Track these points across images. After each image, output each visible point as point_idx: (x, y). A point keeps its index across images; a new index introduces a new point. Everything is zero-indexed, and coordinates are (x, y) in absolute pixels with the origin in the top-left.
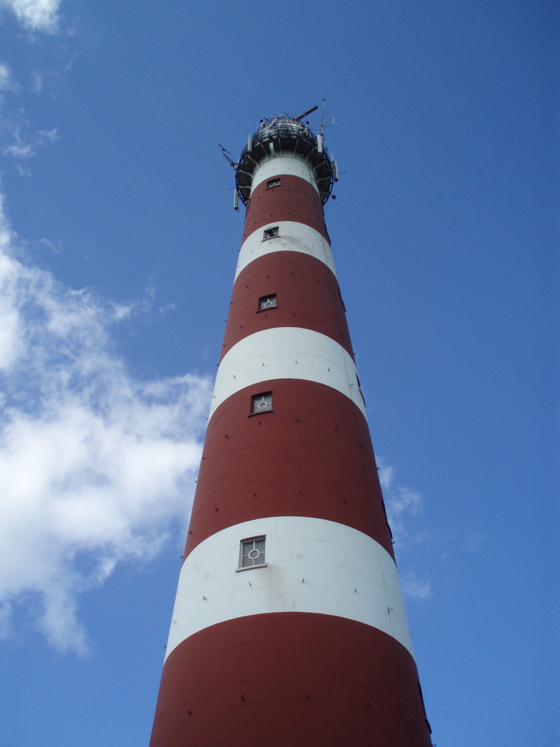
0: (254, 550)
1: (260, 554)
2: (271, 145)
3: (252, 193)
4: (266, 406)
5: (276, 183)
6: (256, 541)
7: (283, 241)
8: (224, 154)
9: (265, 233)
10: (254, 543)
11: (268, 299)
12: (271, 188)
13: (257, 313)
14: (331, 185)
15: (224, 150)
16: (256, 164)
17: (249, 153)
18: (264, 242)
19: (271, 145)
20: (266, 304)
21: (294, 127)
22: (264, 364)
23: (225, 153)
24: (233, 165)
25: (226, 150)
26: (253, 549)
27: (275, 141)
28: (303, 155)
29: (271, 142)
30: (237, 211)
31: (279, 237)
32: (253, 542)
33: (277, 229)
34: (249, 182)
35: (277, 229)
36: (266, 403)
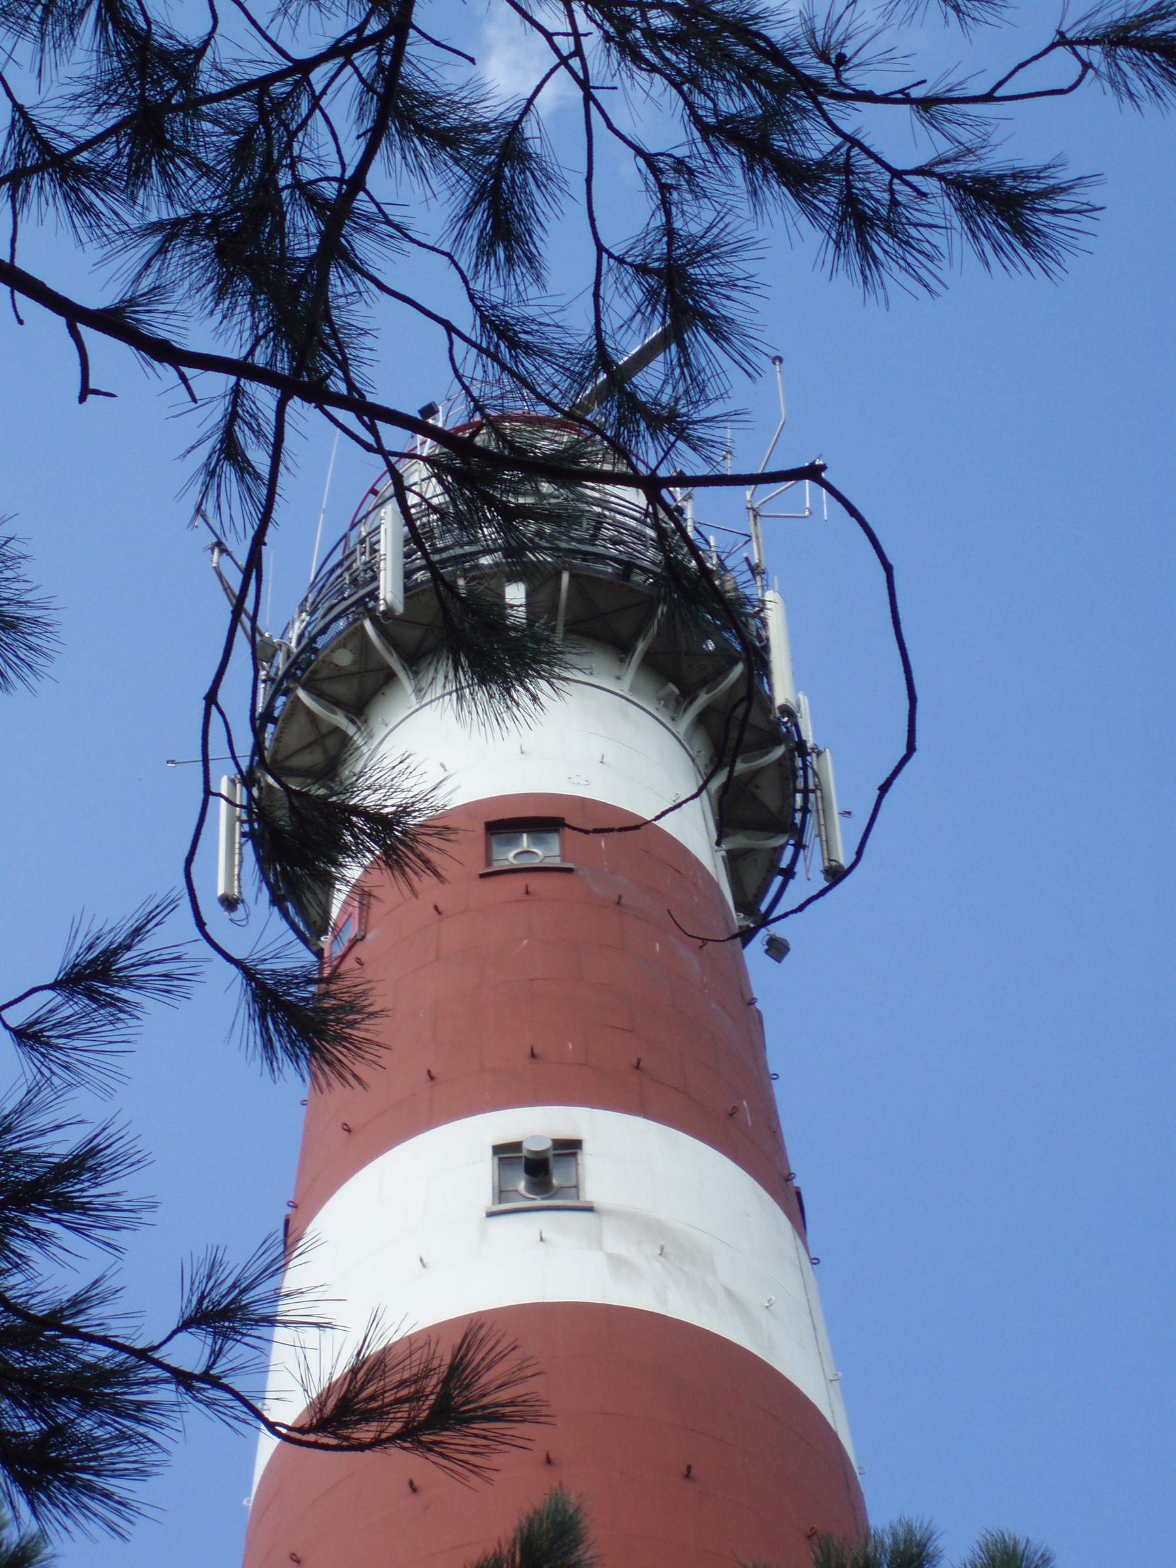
5: (536, 842)
8: (220, 576)
14: (778, 880)
17: (385, 622)
21: (637, 515)
25: (229, 554)
28: (672, 688)
29: (513, 578)
30: (235, 915)
33: (569, 1148)
35: (569, 1148)
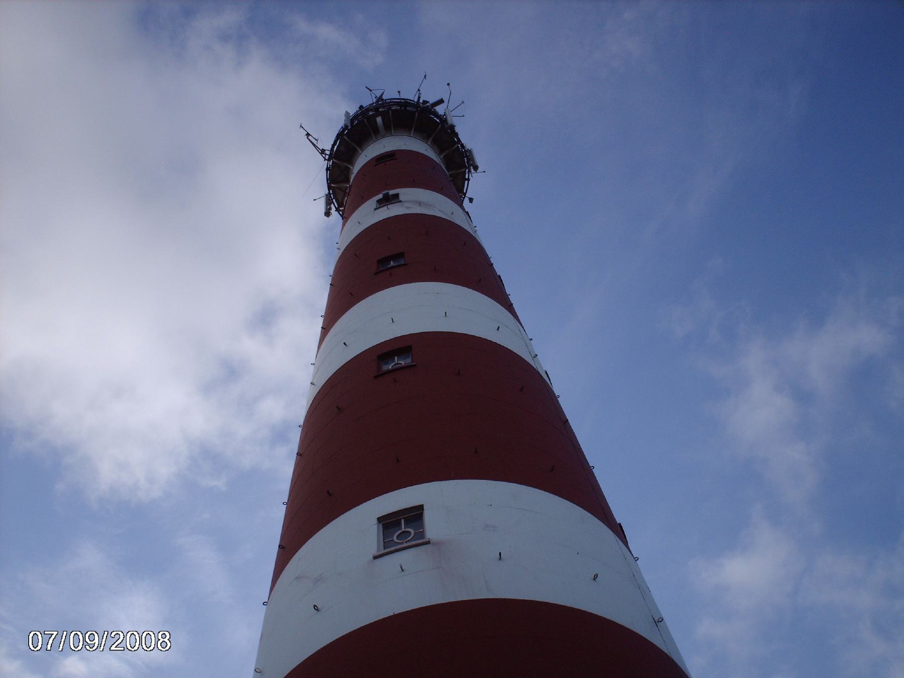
0: (403, 530)
1: (415, 534)
2: (379, 120)
3: (353, 179)
4: (411, 537)
6: (404, 518)
7: (406, 204)
9: (381, 525)
10: (403, 521)
11: (396, 358)
12: (389, 372)
13: (376, 274)
15: (308, 135)
16: (358, 149)
18: (377, 210)
19: (379, 120)
20: (397, 533)
22: (403, 568)
23: (310, 137)
24: (323, 152)
26: (402, 529)
27: (384, 115)
29: (378, 116)
31: (428, 543)
32: (401, 519)
33: (415, 515)
34: (348, 171)
36: (412, 531)
